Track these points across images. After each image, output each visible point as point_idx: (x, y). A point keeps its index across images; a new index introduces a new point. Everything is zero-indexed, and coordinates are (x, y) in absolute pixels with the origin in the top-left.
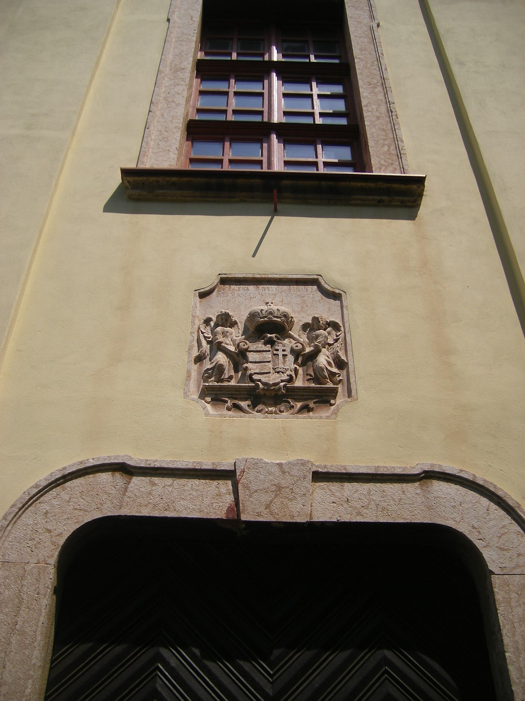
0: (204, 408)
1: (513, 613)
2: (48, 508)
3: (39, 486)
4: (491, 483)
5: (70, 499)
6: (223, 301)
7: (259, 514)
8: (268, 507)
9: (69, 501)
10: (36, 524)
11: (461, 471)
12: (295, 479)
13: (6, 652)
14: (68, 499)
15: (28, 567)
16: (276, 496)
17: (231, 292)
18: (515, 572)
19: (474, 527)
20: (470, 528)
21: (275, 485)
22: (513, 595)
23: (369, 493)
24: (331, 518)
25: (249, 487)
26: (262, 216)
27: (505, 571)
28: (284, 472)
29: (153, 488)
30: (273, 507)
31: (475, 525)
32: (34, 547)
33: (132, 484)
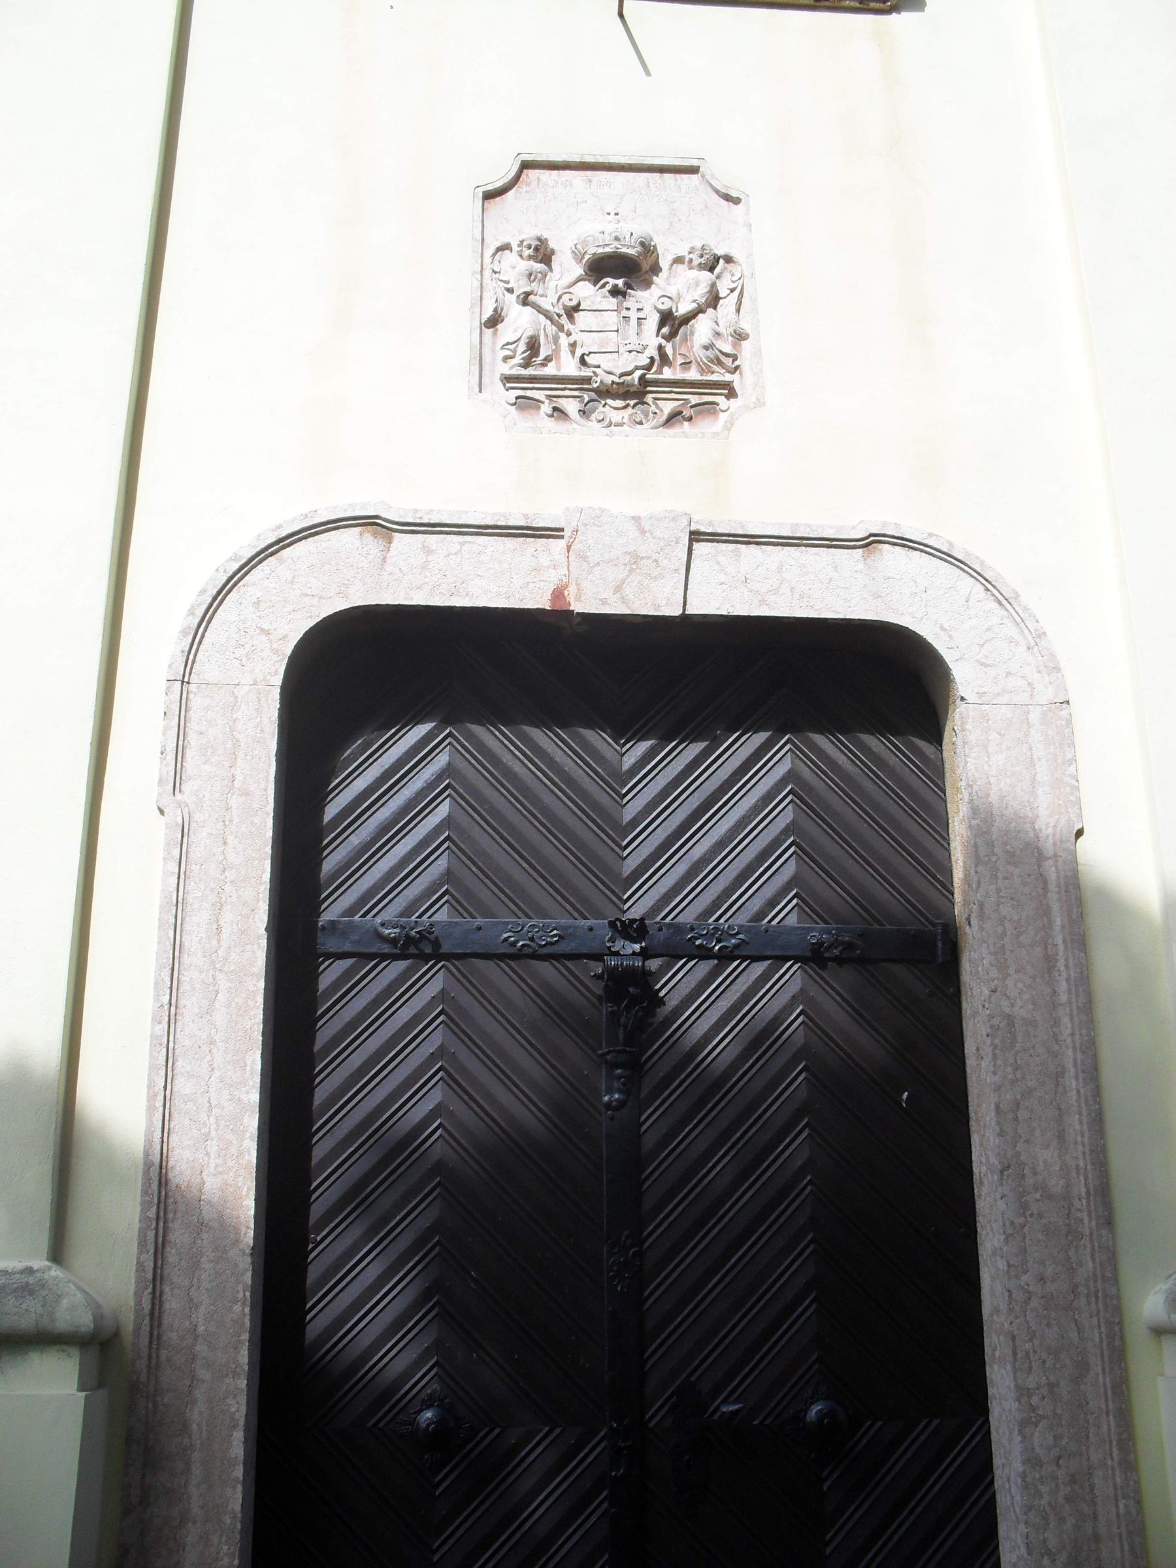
0: (504, 417)
1: (991, 763)
2: (259, 595)
3: (241, 557)
4: (977, 558)
5: (294, 577)
6: (527, 209)
7: (604, 602)
8: (618, 589)
9: (292, 582)
10: (244, 621)
11: (931, 535)
12: (662, 543)
13: (224, 821)
14: (290, 579)
15: (241, 692)
16: (631, 571)
17: (543, 190)
18: (1000, 700)
19: (942, 628)
20: (938, 630)
21: (629, 554)
22: (993, 736)
23: (780, 569)
24: (719, 608)
25: (587, 557)
26: (74, 1530)
27: (984, 700)
28: (643, 532)
29: (430, 558)
30: (628, 591)
31: (946, 626)
32: (244, 660)
33: (393, 551)
